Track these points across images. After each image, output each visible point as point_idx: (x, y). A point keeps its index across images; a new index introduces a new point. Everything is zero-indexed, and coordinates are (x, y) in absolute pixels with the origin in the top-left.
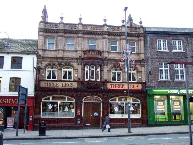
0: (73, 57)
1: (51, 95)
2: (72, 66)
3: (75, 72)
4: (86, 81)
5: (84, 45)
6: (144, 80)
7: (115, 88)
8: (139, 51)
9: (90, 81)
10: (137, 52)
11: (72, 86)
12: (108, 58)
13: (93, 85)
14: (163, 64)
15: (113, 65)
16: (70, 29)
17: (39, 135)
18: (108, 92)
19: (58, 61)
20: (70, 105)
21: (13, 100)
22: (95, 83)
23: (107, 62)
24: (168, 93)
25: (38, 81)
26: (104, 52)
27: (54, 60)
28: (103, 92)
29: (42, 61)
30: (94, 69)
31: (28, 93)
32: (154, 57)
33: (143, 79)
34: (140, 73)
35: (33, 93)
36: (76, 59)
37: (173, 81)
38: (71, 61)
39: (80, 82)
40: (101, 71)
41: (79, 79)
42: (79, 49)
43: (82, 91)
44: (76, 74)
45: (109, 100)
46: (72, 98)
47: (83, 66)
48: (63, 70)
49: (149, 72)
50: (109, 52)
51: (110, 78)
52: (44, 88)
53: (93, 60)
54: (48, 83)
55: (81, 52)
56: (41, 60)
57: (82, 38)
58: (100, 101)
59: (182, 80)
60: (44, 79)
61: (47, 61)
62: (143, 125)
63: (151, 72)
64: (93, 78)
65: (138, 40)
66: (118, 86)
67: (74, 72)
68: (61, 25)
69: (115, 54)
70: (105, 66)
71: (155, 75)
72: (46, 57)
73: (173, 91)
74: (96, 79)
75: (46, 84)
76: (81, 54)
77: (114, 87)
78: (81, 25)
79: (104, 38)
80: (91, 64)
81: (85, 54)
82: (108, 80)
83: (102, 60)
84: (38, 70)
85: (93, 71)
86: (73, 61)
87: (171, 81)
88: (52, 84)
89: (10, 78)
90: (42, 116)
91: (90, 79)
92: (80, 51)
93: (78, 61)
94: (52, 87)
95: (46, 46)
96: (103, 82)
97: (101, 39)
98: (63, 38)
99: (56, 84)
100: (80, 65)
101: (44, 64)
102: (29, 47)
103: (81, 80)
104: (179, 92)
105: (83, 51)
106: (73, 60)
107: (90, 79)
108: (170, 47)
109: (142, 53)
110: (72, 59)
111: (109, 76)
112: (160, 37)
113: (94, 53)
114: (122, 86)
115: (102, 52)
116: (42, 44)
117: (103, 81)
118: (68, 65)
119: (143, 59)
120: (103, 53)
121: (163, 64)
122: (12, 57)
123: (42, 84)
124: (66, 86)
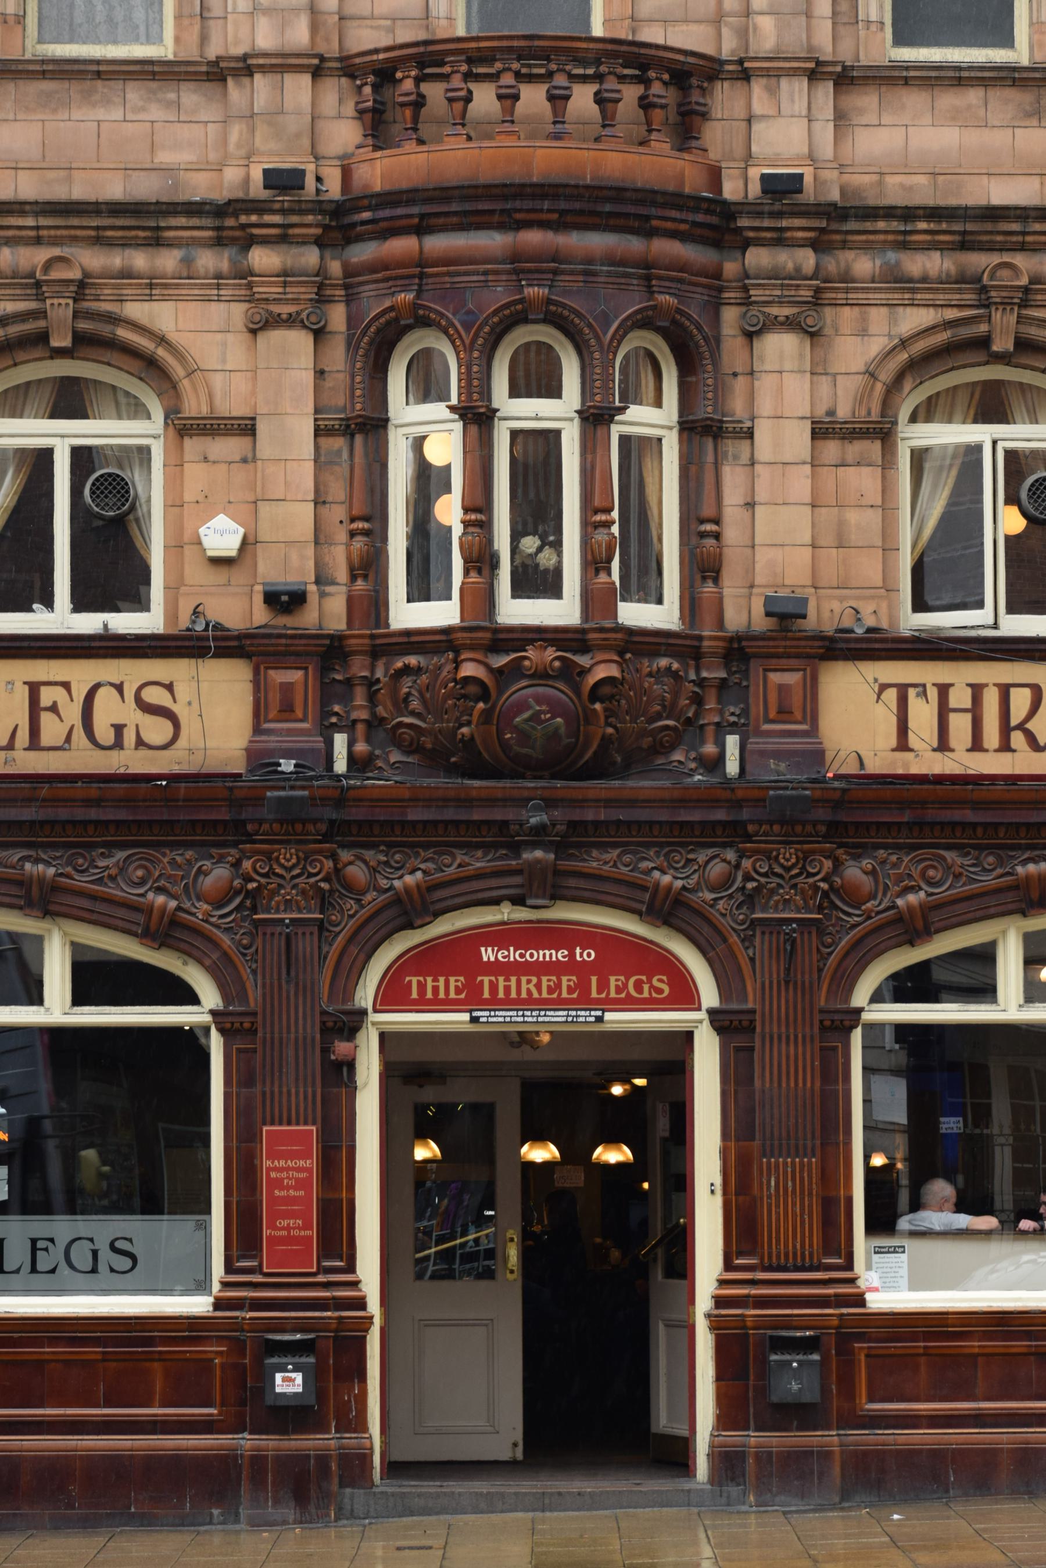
0: (145, 188)
3: (196, 476)
4: (416, 641)
7: (977, 745)
11: (157, 731)
12: (824, 186)
15: (914, 319)
18: (835, 830)
21: (536, 995)
22: (570, 674)
23: (807, 259)
28: (733, 833)
30: (558, 412)
36: (202, 229)
38: (116, 260)
39: (299, 651)
40: (707, 431)
41: (285, 601)
42: (265, 38)
43: (336, 820)
44: (228, 508)
45: (847, 982)
47: (352, 345)
50: (846, 78)
51: (870, 569)
53: (533, 238)
55: (299, 88)
58: (684, 994)
64: (539, 581)
67: (175, 465)
69: (973, 96)
70: (780, 347)
74: (597, 601)
76: (322, 133)
77: (943, 745)
80: (517, 316)
81: (377, 126)
82: (825, 614)
83: (719, 224)
85: (537, 453)
86: (168, 261)
88: (1020, 701)
91: (480, 600)
92: (281, 64)
93: (263, 259)
96: (739, 651)
100: (300, 341)
103: (330, 612)
105: (349, 68)
106: (156, 241)
107: (480, 600)
110: (141, 221)
111: (863, 522)
117: (735, 619)
118: (1002, 344)
120: (725, 100)
124: (34, 743)
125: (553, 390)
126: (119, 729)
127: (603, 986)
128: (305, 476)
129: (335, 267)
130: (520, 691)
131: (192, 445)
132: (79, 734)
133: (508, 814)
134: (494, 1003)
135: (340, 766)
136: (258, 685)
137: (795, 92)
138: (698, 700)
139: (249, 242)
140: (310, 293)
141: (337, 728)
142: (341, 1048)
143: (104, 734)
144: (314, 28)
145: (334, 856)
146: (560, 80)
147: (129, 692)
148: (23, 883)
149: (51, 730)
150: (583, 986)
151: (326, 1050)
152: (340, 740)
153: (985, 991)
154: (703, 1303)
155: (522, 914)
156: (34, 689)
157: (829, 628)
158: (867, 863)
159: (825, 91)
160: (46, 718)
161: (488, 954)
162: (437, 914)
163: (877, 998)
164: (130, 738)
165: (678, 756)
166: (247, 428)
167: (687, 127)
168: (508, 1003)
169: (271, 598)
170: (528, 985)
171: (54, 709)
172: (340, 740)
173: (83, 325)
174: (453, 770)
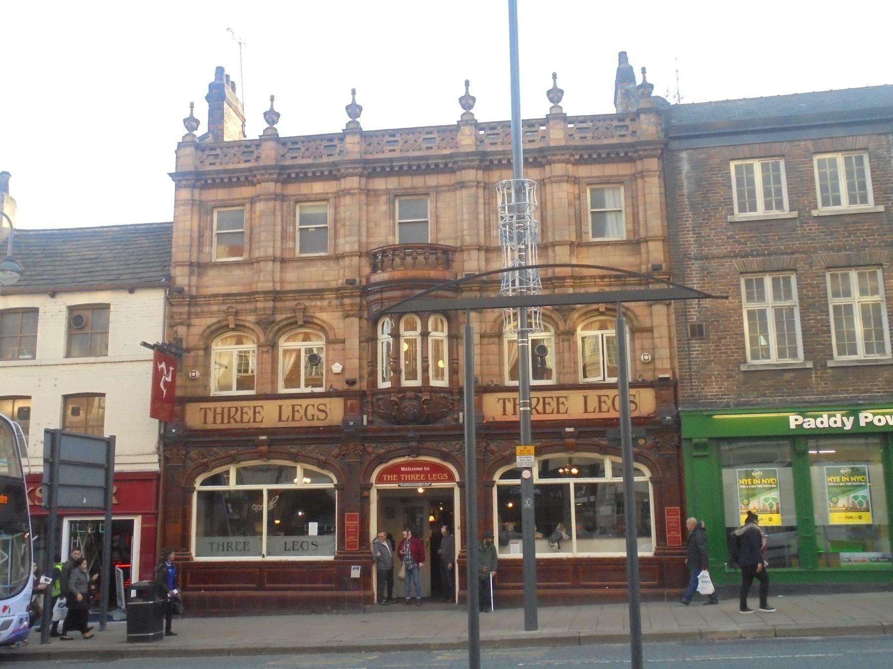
0: (321, 286)
1: (233, 460)
2: (322, 327)
3: (638, 343)
5: (372, 225)
6: (664, 371)
8: (635, 231)
9: (397, 388)
10: (632, 238)
11: (322, 416)
13: (410, 407)
14: (768, 281)
16: (310, 161)
17: (130, 640)
19: (255, 310)
20: (316, 505)
22: (418, 398)
23: (478, 294)
24: (793, 425)
25: (167, 404)
26: (461, 250)
27: (240, 307)
29: (189, 313)
31: (117, 460)
32: (715, 251)
33: (659, 365)
34: (645, 335)
35: (156, 458)
37: (821, 365)
41: (351, 383)
42: (347, 249)
43: (363, 436)
45: (194, 482)
46: (325, 472)
48: (284, 344)
49: (692, 327)
52: (201, 431)
54: (219, 411)
56: (186, 309)
57: (363, 198)
58: (451, 478)
59: (872, 357)
60: (200, 392)
61: (211, 313)
62: (666, 591)
63: (700, 327)
64: (412, 375)
65: (634, 177)
66: (232, 414)
68: (467, 130)
71: (720, 339)
72: (205, 297)
73: (815, 418)
75: (210, 416)
77: (215, 422)
78: (357, 138)
79: (462, 185)
83: (456, 286)
84: (168, 354)
86: (325, 303)
87: (810, 365)
88: (233, 411)
89: (66, 398)
90: (197, 555)
91: (426, 379)
92: (351, 255)
93: (347, 301)
94: (233, 425)
95: (206, 249)
97: (449, 190)
98: (278, 203)
99: (251, 413)
100: (356, 320)
101: (201, 324)
102: (135, 258)
103: (363, 385)
104: (852, 419)
108: (801, 187)
109: (655, 239)
110: (318, 293)
111: (494, 358)
112: (746, 150)
113: (415, 259)
114: (554, 404)
115: (454, 250)
116: (187, 242)
118: (232, 326)
119: (657, 268)
120: (457, 256)
121: (768, 281)
122: (71, 309)
123: (194, 417)
125: (414, 329)
126: (313, 416)
127: (431, 476)
128: (356, 352)
129: (364, 302)
130: (406, 403)
131: (331, 346)
132: (304, 417)
133: (403, 434)
134: (405, 481)
135: (365, 423)
136: (345, 404)
137: (474, 254)
138: (453, 404)
139: (343, 297)
140: (358, 308)
141: (364, 414)
142: (366, 493)
143: (310, 417)
144: (359, 246)
145: (363, 445)
146: (427, 254)
147: (316, 406)
148: (289, 453)
149: (604, 407)
150: (426, 477)
151: (362, 494)
152: (365, 417)
153: (226, 482)
154: (457, 558)
155: (411, 459)
156: (599, 397)
157: (484, 384)
158: (496, 444)
159: (483, 253)
160: (603, 404)
161: (403, 469)
162: (391, 459)
163: (501, 478)
164: (316, 418)
165: (448, 418)
166: (343, 342)
167: (448, 264)
168: (408, 481)
169: (348, 382)
170: (413, 476)
171: (549, 404)
172: (365, 417)
173: (306, 319)
174: (393, 423)
